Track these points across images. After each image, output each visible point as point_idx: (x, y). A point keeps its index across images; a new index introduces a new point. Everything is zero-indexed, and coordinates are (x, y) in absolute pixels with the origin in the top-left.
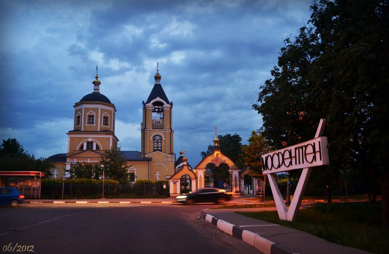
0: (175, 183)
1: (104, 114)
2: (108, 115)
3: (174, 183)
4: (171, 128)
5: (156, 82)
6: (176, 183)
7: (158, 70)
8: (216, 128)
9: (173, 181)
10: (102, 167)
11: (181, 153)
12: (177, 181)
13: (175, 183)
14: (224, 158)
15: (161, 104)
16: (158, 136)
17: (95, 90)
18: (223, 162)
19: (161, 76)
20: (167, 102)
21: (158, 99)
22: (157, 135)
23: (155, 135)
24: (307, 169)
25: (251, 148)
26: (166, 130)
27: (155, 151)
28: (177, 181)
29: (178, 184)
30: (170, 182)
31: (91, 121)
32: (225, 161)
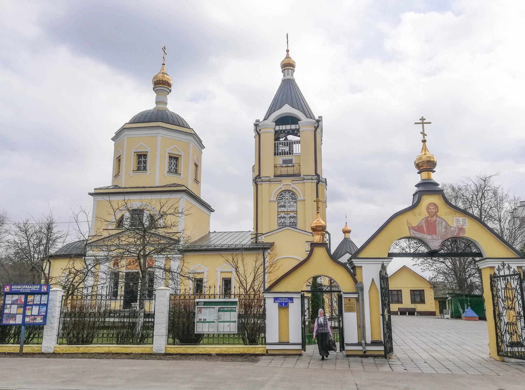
0: (283, 305)
1: (169, 149)
2: (282, 196)
3: (280, 305)
4: (318, 172)
5: (284, 76)
6: (286, 304)
7: (288, 51)
8: (423, 123)
9: (276, 299)
10: (38, 256)
11: (346, 232)
12: (291, 299)
13: (283, 305)
14: (458, 221)
15: (294, 120)
16: (289, 191)
17: (157, 103)
18: (455, 234)
19: (294, 62)
20: (308, 114)
21: (287, 109)
22: (285, 191)
23: (281, 190)
24: (312, 279)
25: (416, 313)
26: (305, 177)
27: (282, 226)
28: (291, 299)
29: (295, 308)
30: (267, 301)
31: (142, 165)
32: (461, 229)
